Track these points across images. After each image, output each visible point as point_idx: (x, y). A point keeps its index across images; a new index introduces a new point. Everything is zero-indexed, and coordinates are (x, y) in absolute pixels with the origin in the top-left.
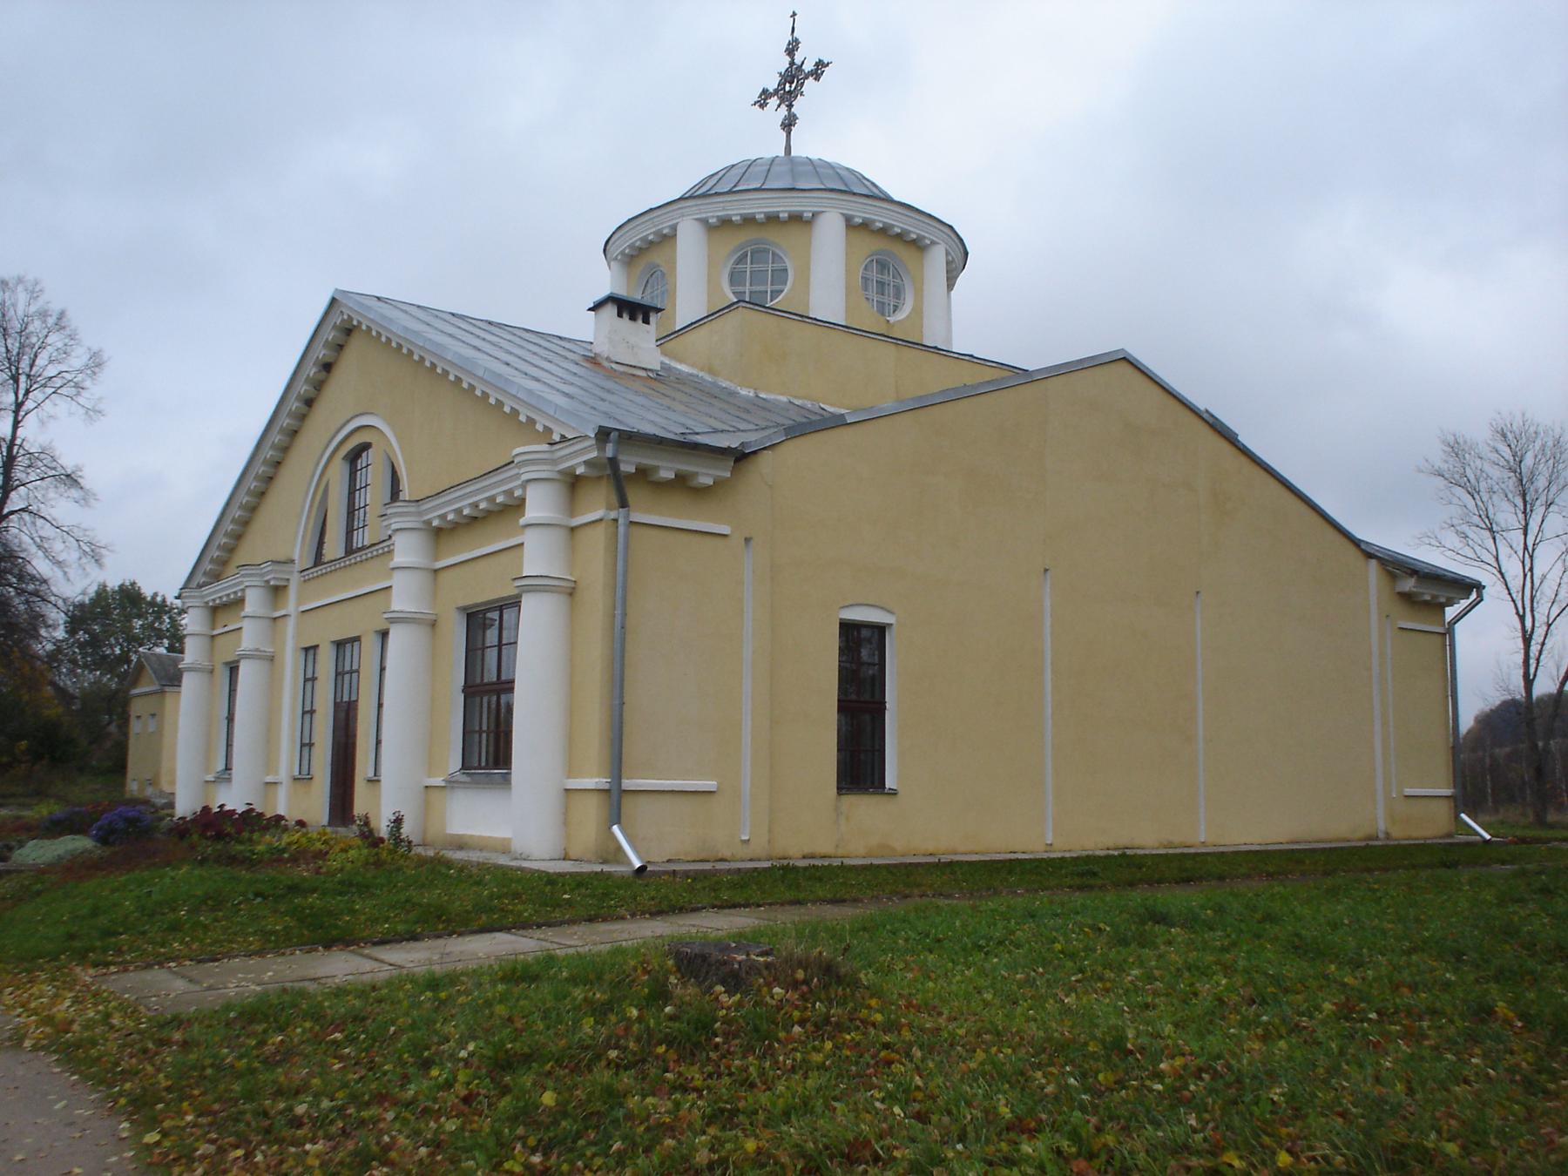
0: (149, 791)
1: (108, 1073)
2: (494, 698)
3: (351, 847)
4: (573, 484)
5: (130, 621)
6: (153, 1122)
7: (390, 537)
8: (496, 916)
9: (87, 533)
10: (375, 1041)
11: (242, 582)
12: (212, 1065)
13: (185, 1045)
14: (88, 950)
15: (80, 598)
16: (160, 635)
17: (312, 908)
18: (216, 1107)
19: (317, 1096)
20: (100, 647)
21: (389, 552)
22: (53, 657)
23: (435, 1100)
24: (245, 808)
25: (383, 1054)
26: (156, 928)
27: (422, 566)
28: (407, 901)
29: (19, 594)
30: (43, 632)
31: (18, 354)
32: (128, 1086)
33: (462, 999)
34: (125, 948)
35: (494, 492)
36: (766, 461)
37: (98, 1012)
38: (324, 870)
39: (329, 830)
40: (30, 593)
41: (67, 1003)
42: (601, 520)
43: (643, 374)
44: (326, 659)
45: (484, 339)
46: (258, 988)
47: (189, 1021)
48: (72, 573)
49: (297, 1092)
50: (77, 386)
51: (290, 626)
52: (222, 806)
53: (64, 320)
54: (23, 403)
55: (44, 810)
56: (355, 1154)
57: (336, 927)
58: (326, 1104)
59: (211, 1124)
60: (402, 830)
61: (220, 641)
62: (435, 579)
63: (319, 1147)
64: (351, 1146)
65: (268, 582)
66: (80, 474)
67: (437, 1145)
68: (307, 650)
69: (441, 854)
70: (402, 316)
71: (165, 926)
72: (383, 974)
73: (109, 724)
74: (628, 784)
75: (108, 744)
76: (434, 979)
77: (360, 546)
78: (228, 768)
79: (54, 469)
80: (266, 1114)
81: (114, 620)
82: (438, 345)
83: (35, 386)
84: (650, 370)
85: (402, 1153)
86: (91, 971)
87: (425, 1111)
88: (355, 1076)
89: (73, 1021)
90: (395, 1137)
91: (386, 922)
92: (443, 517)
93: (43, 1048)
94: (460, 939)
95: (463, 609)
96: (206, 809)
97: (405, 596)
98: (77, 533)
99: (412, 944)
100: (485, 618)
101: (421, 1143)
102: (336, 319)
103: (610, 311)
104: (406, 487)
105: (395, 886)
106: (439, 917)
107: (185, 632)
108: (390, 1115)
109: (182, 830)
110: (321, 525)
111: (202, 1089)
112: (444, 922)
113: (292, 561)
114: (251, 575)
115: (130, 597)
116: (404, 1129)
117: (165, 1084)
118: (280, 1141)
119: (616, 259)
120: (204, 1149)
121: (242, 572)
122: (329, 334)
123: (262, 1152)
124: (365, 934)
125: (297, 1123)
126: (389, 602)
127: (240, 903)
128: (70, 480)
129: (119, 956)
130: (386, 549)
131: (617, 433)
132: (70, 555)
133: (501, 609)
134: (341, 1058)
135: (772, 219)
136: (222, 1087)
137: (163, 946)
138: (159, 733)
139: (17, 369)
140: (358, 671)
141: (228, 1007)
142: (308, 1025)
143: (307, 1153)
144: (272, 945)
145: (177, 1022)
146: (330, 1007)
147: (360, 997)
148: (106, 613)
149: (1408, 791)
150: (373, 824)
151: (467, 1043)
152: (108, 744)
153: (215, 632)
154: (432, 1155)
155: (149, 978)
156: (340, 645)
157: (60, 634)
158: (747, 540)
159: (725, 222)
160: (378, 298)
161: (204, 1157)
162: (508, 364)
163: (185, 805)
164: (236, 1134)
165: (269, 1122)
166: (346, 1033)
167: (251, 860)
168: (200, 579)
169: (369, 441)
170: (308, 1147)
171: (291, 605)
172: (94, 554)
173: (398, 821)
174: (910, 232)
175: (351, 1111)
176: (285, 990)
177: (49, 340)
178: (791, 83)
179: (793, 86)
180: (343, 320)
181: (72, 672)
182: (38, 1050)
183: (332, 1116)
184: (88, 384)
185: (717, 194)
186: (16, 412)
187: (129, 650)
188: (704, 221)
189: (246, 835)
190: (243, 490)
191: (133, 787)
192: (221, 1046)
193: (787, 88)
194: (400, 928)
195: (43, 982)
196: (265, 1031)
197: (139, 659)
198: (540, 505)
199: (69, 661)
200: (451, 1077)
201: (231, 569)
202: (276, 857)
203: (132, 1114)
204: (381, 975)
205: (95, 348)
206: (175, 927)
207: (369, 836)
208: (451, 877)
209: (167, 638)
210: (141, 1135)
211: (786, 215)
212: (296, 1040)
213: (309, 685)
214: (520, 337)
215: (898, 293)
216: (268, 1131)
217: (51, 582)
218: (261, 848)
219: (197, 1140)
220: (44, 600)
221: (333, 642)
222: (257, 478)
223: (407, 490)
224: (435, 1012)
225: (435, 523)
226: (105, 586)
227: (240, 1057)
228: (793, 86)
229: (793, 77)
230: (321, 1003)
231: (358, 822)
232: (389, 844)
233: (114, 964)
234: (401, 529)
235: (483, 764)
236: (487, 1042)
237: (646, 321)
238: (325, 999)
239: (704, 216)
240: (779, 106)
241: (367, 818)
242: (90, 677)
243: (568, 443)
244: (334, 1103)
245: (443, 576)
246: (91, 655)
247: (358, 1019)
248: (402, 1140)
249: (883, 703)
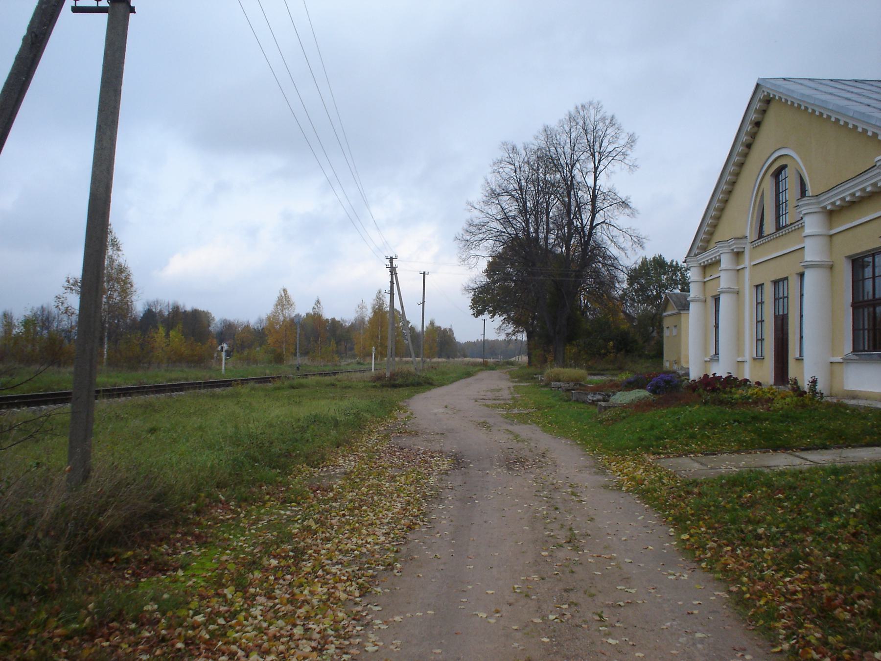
0: (675, 367)
1: (662, 505)
2: (871, 309)
3: (787, 396)
5: (660, 277)
6: (686, 530)
7: (802, 218)
8: (876, 438)
9: (635, 231)
10: (801, 500)
11: (718, 251)
12: (714, 506)
13: (700, 494)
14: (650, 446)
15: (634, 266)
16: (676, 283)
17: (765, 428)
18: (716, 525)
19: (769, 525)
20: (646, 291)
21: (802, 227)
22: (622, 297)
23: (836, 533)
24: (727, 375)
25: (806, 507)
26: (682, 437)
27: (820, 234)
28: (820, 427)
29: (603, 266)
30: (617, 285)
31: (593, 141)
32: (672, 511)
33: (853, 481)
34: (668, 446)
35: (825, 204)
37: (657, 476)
38: (772, 408)
39: (774, 387)
40: (609, 266)
41: (641, 471)
44: (769, 290)
45: (852, 92)
46: (737, 470)
47: (701, 483)
48: (629, 253)
49: (759, 522)
50: (623, 154)
51: (747, 273)
52: (714, 374)
53: (614, 120)
54: (598, 167)
55: (624, 377)
56: (790, 555)
57: (780, 440)
58: (774, 529)
59: (714, 533)
60: (817, 387)
61: (709, 284)
63: (771, 550)
64: (788, 551)
65: (733, 250)
66: (629, 200)
67: (836, 556)
68: (757, 286)
69: (841, 401)
70: (799, 87)
71: (688, 436)
72: (806, 466)
73: (653, 331)
75: (653, 343)
76: (836, 469)
77: (784, 225)
78: (717, 354)
79: (616, 199)
80: (742, 531)
81: (652, 276)
82: (823, 101)
83: (603, 158)
85: (817, 558)
86: (652, 457)
87: (830, 539)
88: (790, 517)
89: (645, 480)
90: (812, 549)
91: (808, 438)
92: (833, 204)
93: (631, 491)
94: (853, 450)
95: (848, 257)
96: (706, 376)
97: (813, 252)
98: (630, 232)
99: (825, 451)
100: (863, 261)
101: (827, 554)
102: (760, 95)
105: (813, 419)
106: (840, 437)
107: (689, 281)
108: (810, 539)
109: (694, 387)
110: (761, 214)
111: (709, 516)
112: (843, 439)
113: (746, 237)
114: (722, 247)
115: (659, 263)
116: (818, 546)
117: (690, 512)
118: (750, 545)
120: (710, 544)
121: (719, 246)
122: (757, 105)
123: (740, 549)
124: (796, 444)
125: (759, 537)
127: (726, 425)
128: (624, 204)
129: (664, 450)
130: (800, 226)
132: (627, 244)
133: (873, 255)
134: (782, 508)
136: (719, 516)
137: (687, 446)
138: (679, 335)
139: (594, 150)
140: (787, 297)
141: (722, 477)
142: (764, 489)
143: (764, 552)
144: (744, 448)
145: (695, 483)
146: (776, 481)
147: (793, 477)
148: (648, 274)
150: (800, 383)
151: (855, 504)
152: (653, 343)
154: (834, 561)
155: (680, 461)
156: (776, 283)
157: (625, 285)
160: (784, 79)
161: (710, 549)
162: (869, 106)
163: (695, 374)
164: (727, 539)
165: (744, 535)
166: (785, 495)
167: (731, 403)
168: (696, 251)
169: (784, 163)
170: (764, 549)
171: (747, 262)
172: (639, 242)
173: (814, 382)
175: (788, 534)
176: (751, 471)
177: (608, 132)
180: (764, 95)
181: (632, 305)
182: (628, 492)
183: (778, 536)
184: (629, 152)
186: (595, 172)
187: (661, 292)
189: (728, 389)
191: (667, 365)
192: (718, 496)
194: (817, 442)
195: (630, 461)
196: (741, 491)
197: (666, 296)
199: (631, 299)
200: (845, 521)
201: (712, 244)
202: (745, 401)
203: (674, 525)
204: (805, 466)
205: (631, 133)
206: (693, 436)
207: (797, 390)
208: (846, 414)
209: (680, 284)
210: (680, 535)
212: (757, 496)
213: (760, 306)
214: (876, 86)
216: (743, 540)
217: (619, 259)
218: (737, 396)
219: (707, 540)
220: (616, 268)
221: (797, 274)
222: (723, 192)
223: (810, 190)
224: (836, 487)
225: (829, 207)
226: (646, 259)
227: (728, 503)
230: (771, 478)
231: (790, 382)
232: (809, 395)
233: (663, 454)
234: (810, 213)
235: (866, 349)
236: (867, 505)
238: (774, 477)
241: (796, 380)
242: (642, 307)
244: (778, 529)
245: (835, 238)
246: (641, 295)
247: (793, 488)
248: (816, 551)
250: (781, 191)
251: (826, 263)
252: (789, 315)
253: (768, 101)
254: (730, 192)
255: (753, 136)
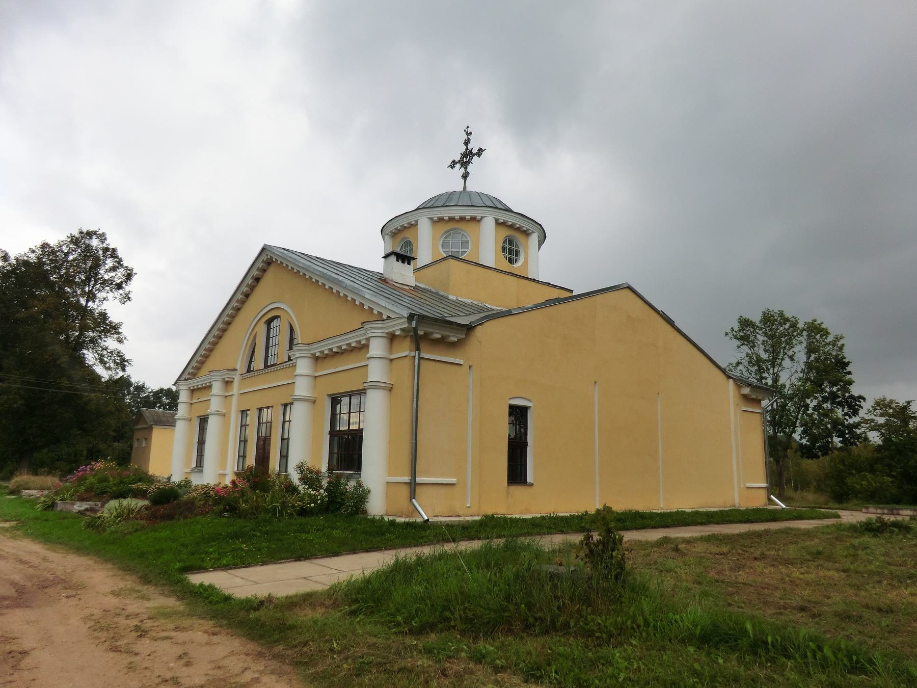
4: (392, 338)
36: (479, 331)
42: (407, 356)
43: (407, 288)
44: (252, 419)
51: (234, 400)
62: (315, 381)
68: (242, 412)
74: (418, 480)
77: (272, 363)
84: (410, 286)
97: (302, 388)
102: (264, 257)
103: (394, 258)
104: (299, 336)
119: (388, 234)
121: (212, 374)
122: (260, 264)
126: (293, 390)
131: (417, 316)
135: (462, 219)
149: (748, 485)
153: (193, 402)
158: (470, 367)
159: (441, 220)
168: (186, 376)
171: (235, 389)
174: (509, 221)
178: (466, 158)
179: (468, 159)
180: (267, 258)
185: (433, 207)
188: (431, 219)
190: (211, 335)
193: (465, 160)
198: (377, 348)
211: (469, 217)
215: (517, 254)
221: (282, 404)
228: (468, 159)
229: (468, 155)
237: (409, 264)
239: (432, 216)
240: (460, 168)
243: (391, 320)
249: (527, 443)
250: (271, 336)
251: (312, 398)
252: (272, 437)
253: (269, 263)
254: (220, 337)
255: (252, 288)
